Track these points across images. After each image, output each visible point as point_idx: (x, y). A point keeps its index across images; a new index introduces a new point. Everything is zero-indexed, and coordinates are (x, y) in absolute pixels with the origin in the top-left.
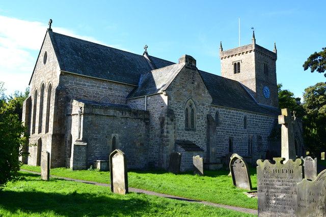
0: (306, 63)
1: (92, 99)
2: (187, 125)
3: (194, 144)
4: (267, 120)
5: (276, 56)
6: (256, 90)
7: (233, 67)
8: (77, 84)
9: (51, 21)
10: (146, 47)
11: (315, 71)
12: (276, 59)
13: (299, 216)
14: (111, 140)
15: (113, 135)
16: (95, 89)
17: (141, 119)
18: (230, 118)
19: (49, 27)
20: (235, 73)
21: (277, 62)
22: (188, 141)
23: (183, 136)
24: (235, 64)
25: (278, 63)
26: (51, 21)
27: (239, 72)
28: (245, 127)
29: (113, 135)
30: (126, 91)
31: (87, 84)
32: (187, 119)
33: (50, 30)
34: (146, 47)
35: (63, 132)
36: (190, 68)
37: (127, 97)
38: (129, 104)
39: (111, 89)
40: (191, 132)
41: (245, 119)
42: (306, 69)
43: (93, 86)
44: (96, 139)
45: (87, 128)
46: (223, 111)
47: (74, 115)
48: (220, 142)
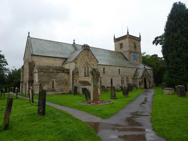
0: (154, 41)
1: (46, 65)
2: (85, 74)
3: (89, 82)
4: (132, 70)
5: (141, 39)
6: (163, 53)
7: (120, 46)
8: (39, 59)
9: (29, 32)
10: (74, 41)
11: (159, 44)
12: (140, 41)
13: (16, 140)
14: (52, 82)
15: (52, 80)
16: (48, 60)
17: (66, 73)
18: (111, 70)
19: (28, 35)
20: (121, 48)
21: (141, 42)
22: (86, 81)
23: (83, 79)
24: (121, 44)
25: (142, 42)
26: (29, 32)
28: (119, 73)
29: (52, 80)
30: (62, 61)
31: (44, 59)
32: (85, 72)
34: (74, 41)
35: (33, 80)
36: (86, 50)
37: (63, 63)
38: (64, 66)
39: (55, 60)
40: (87, 77)
41: (119, 70)
42: (153, 44)
43: (46, 59)
44: (45, 82)
45: (39, 78)
46: (107, 67)
47: (128, 33)
48: (106, 81)
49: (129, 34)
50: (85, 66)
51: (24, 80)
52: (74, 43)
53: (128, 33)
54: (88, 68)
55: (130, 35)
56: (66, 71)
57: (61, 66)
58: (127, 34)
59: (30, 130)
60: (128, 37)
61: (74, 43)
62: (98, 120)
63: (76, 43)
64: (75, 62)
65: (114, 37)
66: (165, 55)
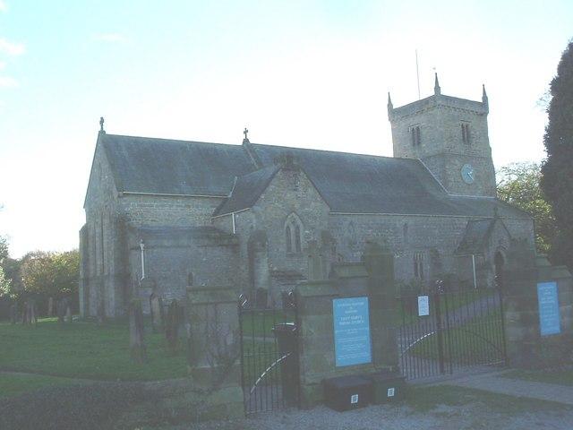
2: (289, 249)
8: (141, 206)
19: (100, 129)
20: (414, 145)
21: (489, 118)
25: (491, 119)
26: (102, 118)
27: (419, 143)
30: (212, 207)
32: (289, 241)
33: (102, 132)
34: (246, 132)
38: (222, 224)
39: (189, 207)
43: (163, 206)
47: (437, 88)
49: (444, 92)
50: (286, 223)
51: (92, 272)
52: (246, 141)
53: (437, 88)
54: (298, 227)
55: (412, 106)
56: (226, 242)
57: (209, 224)
58: (432, 93)
59: (152, 296)
60: (438, 103)
61: (246, 141)
62: (244, 247)
63: (251, 141)
64: (253, 212)
65: (390, 105)
66: (409, 154)
